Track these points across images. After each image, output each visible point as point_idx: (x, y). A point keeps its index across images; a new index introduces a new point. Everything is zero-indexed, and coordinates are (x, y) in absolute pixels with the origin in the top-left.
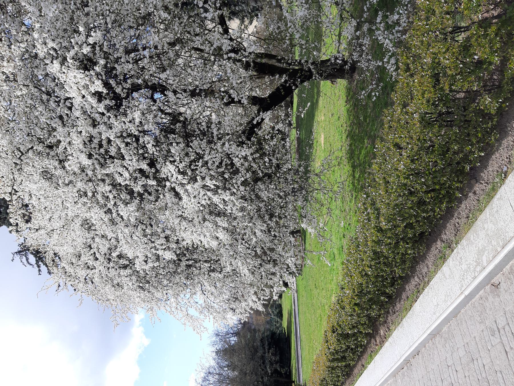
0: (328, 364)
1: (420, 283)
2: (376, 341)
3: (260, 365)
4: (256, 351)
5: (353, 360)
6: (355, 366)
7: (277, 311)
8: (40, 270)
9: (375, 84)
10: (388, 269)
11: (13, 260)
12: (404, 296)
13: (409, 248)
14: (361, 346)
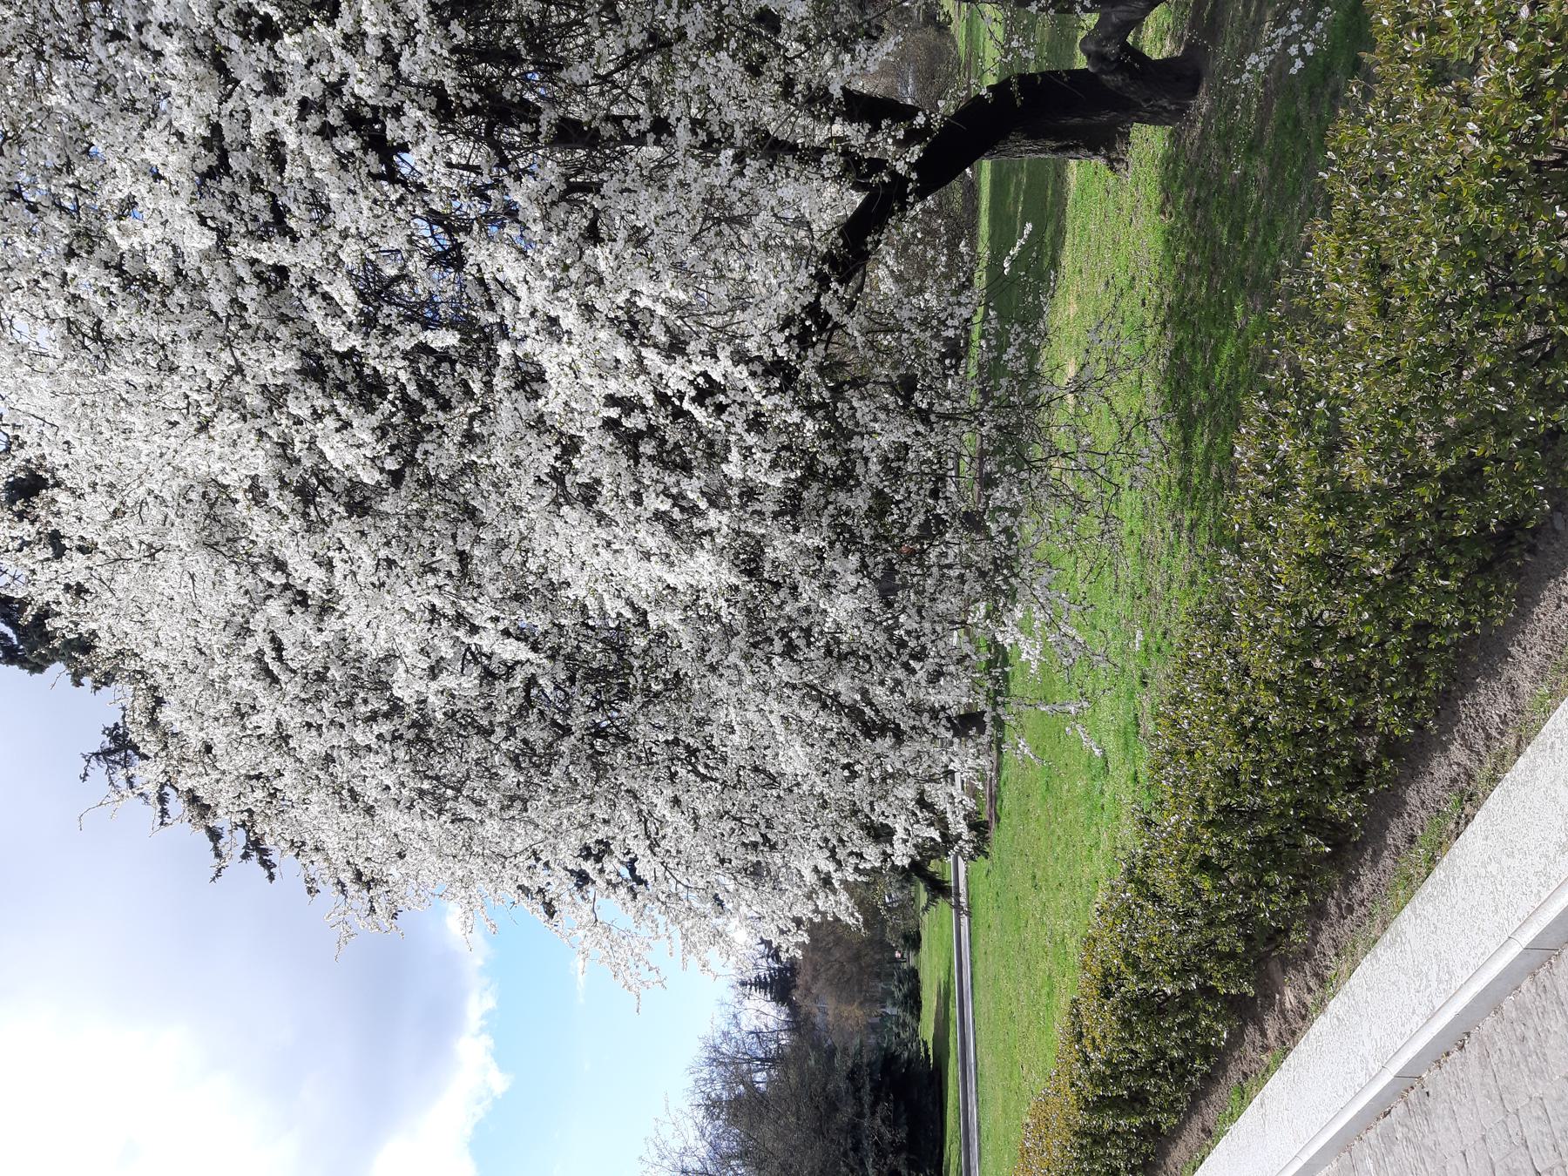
0: (1081, 1119)
1: (1474, 765)
2: (1264, 1034)
3: (845, 1154)
4: (833, 1107)
5: (1171, 1109)
6: (1175, 1134)
7: (905, 989)
8: (164, 812)
9: (1300, 20)
10: (1351, 703)
11: (84, 777)
12: (1395, 834)
13: (1446, 592)
14: (1206, 1052)
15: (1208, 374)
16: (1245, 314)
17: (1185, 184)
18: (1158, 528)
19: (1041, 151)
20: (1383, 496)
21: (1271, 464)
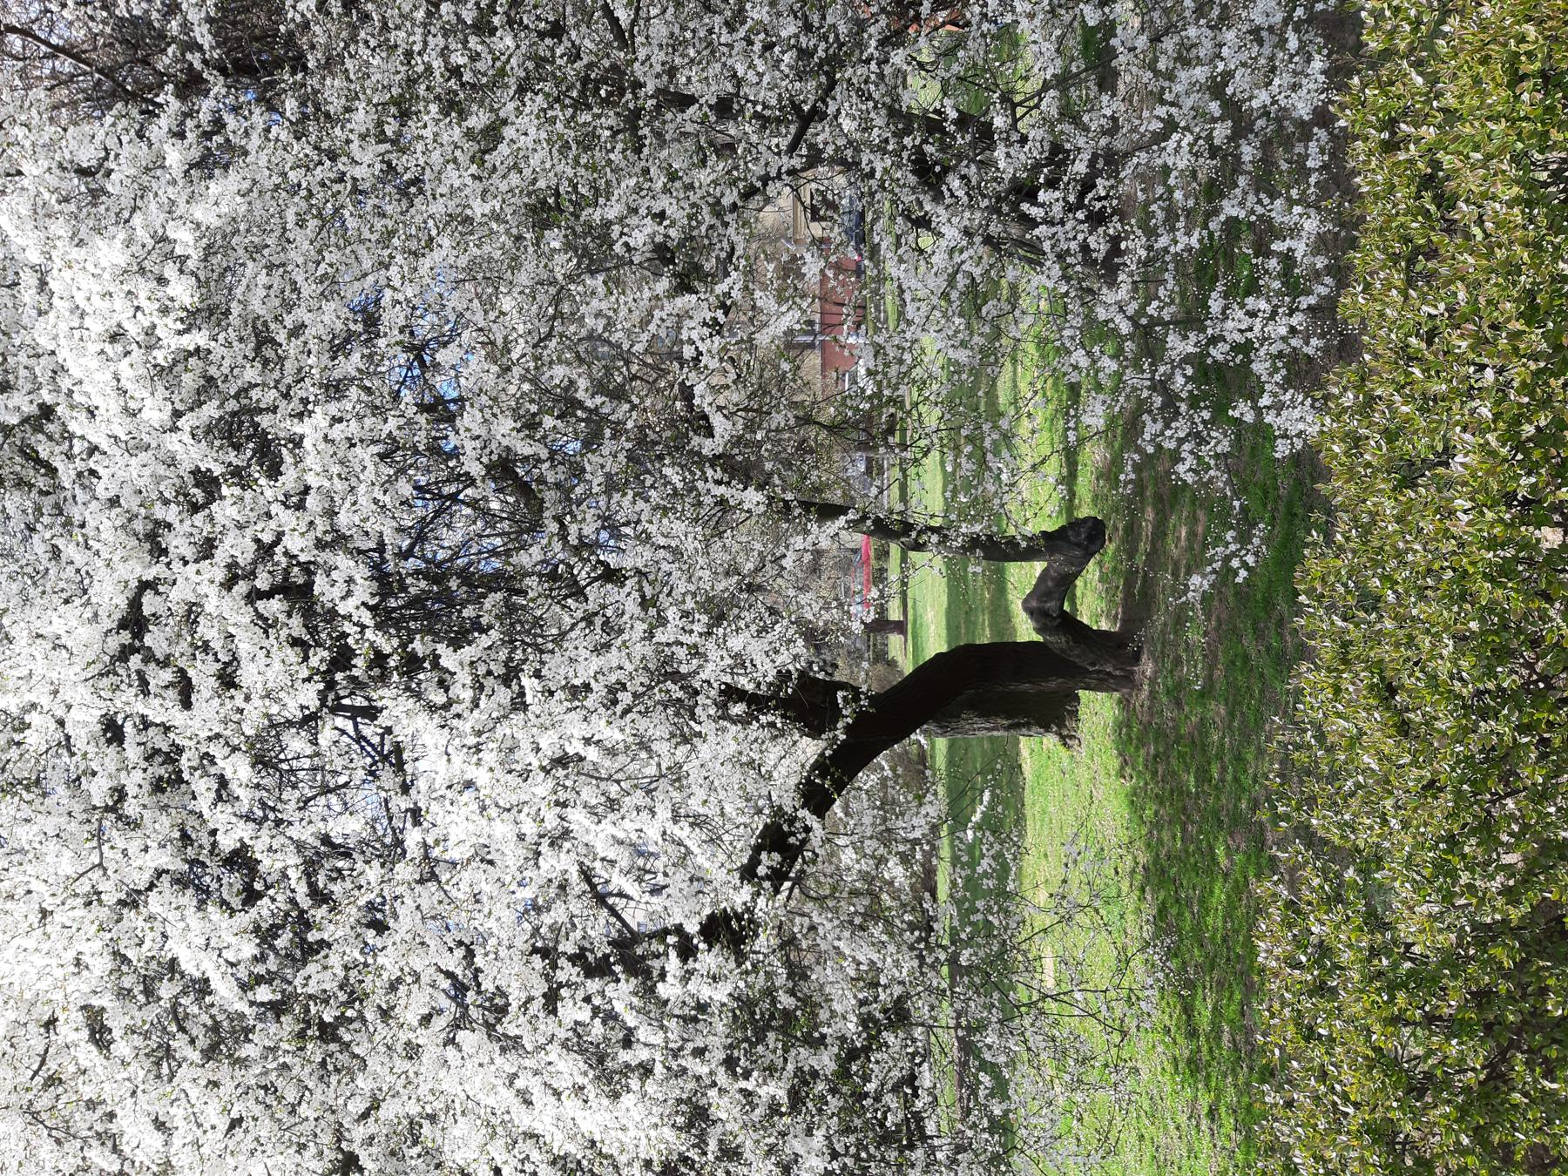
15: (1198, 929)
16: (1229, 855)
17: (1142, 743)
18: (1172, 1127)
19: (993, 729)
20: (1453, 961)
21: (1305, 953)
